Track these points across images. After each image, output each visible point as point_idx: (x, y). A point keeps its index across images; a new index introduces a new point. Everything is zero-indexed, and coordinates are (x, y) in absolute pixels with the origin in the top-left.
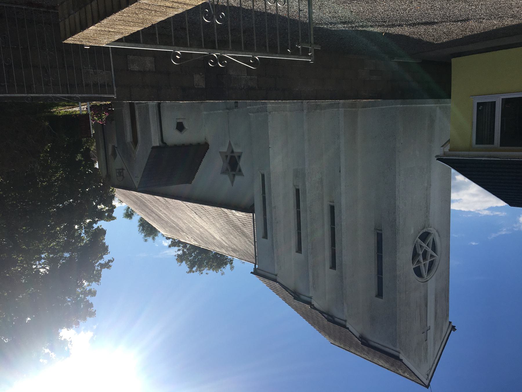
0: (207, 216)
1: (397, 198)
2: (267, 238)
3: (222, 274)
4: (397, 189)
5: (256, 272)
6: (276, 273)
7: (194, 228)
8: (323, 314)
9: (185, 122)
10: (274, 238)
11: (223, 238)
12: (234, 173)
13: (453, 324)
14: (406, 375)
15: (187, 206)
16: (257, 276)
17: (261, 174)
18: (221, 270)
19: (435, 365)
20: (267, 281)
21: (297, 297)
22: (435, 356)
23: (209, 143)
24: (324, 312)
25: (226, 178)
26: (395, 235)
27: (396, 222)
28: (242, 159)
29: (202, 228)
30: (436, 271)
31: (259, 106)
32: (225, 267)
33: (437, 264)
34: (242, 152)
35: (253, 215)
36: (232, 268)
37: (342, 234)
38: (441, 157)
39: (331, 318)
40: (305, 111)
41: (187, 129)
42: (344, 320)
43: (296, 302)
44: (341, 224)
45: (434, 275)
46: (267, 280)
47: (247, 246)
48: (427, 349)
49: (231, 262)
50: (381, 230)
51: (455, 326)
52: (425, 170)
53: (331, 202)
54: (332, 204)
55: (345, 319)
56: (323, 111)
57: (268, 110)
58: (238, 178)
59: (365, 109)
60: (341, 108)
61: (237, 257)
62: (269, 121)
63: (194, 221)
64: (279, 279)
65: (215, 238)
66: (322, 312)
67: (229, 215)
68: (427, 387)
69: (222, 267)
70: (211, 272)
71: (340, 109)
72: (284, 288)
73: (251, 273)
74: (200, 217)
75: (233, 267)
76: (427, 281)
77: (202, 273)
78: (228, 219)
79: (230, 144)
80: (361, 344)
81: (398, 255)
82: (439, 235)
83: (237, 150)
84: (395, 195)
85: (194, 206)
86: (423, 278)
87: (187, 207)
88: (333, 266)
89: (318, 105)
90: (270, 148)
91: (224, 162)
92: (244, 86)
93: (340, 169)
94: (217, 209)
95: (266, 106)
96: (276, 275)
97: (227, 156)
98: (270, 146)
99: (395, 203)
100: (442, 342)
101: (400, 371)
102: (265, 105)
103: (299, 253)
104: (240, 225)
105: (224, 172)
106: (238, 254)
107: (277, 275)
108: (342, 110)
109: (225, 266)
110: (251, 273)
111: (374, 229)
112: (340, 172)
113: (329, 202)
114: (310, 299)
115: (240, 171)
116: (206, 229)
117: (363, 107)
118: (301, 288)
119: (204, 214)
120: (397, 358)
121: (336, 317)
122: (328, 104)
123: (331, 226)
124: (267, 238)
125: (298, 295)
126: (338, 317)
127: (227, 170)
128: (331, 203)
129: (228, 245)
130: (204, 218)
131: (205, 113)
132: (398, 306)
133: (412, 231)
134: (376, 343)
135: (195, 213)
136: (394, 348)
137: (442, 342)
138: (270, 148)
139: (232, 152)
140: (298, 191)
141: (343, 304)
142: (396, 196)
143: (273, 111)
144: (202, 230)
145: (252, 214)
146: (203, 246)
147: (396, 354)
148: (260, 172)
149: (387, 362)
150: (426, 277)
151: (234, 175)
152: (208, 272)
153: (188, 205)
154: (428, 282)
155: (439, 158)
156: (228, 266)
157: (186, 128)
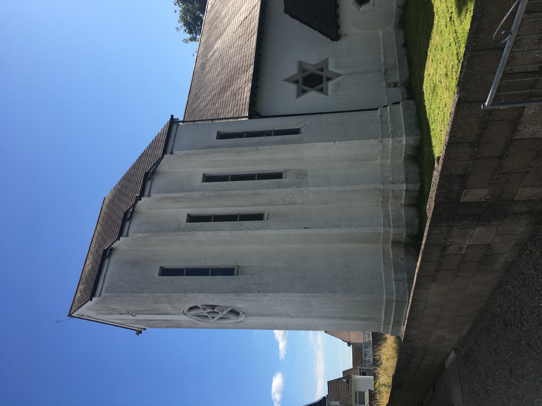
0: (243, 37)
1: (275, 295)
2: (217, 138)
3: (177, 29)
4: (286, 294)
5: (173, 121)
6: (175, 152)
7: (227, 8)
8: (132, 208)
9: (368, 6)
10: (219, 149)
11: (217, 54)
12: (300, 82)
13: (143, 331)
14: (79, 294)
15: (255, 5)
16: (169, 122)
17: (301, 128)
18: (182, 26)
19: (96, 320)
20: (163, 138)
21: (148, 177)
22: (104, 320)
23: (340, 42)
24: (134, 210)
25: (293, 70)
26: (233, 292)
27: (247, 293)
28: (319, 95)
29: (228, 23)
30: (197, 320)
31: (390, 126)
32: (186, 32)
33: (206, 320)
34: (327, 95)
35: (246, 117)
36: (186, 41)
37: (230, 230)
38: (327, 404)
39: (129, 216)
40: (382, 187)
41: (359, 10)
42: (128, 233)
43: (141, 173)
44: (241, 230)
45: (192, 319)
46: (164, 137)
47: (209, 90)
48: (111, 314)
49: (193, 39)
50: (238, 274)
51: (141, 333)
52: (309, 314)
53: (268, 215)
54: (265, 216)
55: (130, 234)
56: (380, 204)
57: (385, 139)
58: (293, 88)
59: (382, 253)
60: (384, 230)
61: (196, 68)
62: (369, 141)
63: (236, 11)
64: (166, 157)
65: (217, 39)
66: (134, 206)
67: (245, 74)
68: (70, 315)
69: (185, 29)
70: (178, 14)
71: (382, 228)
72: (157, 162)
73: (172, 115)
74: (241, 24)
75: (187, 42)
76: (185, 314)
77: (175, 4)
78: (241, 70)
79: (338, 75)
80: (104, 250)
81: (211, 295)
82: (238, 322)
83: (331, 85)
84: (279, 292)
85: (255, 17)
86: (188, 312)
87: (254, 5)
88: (192, 219)
89: (389, 200)
90: (335, 142)
91: (314, 66)
92: (451, 242)
93: (308, 228)
94: (252, 57)
95: (389, 137)
96: (171, 153)
97: (322, 70)
98: (336, 142)
99: (270, 292)
100: (122, 324)
101: (81, 287)
102: (391, 135)
103: (203, 178)
104: (233, 87)
105: (301, 67)
106: (200, 71)
107: (172, 154)
108: (381, 230)
109: (187, 31)
110: (172, 115)
111: (238, 266)
112: (305, 228)
113: (267, 212)
114: (148, 195)
115: (304, 92)
116: (227, 30)
117: (383, 251)
118: (158, 183)
119: (246, 32)
120: (93, 295)
121: (131, 223)
122: (389, 211)
123: (239, 216)
124: (217, 138)
125: (151, 176)
126: (131, 225)
127: (304, 71)
128: (267, 215)
129: (209, 59)
130: (240, 30)
131: (381, 34)
132: (152, 294)
133: (238, 306)
134: (107, 268)
135: (247, 17)
136: (104, 290)
137: (122, 324)
138: (335, 142)
139: (329, 79)
140: (278, 176)
141: (147, 232)
142: (278, 294)
143: (382, 146)
144: (225, 22)
145: (247, 115)
146: (206, 18)
147: (98, 293)
148: (303, 127)
149: (90, 272)
150: (189, 313)
151: (297, 82)
152: (178, 12)
153: (256, 8)
154: (185, 316)
155: (327, 400)
156: (189, 36)
157: (361, 9)
